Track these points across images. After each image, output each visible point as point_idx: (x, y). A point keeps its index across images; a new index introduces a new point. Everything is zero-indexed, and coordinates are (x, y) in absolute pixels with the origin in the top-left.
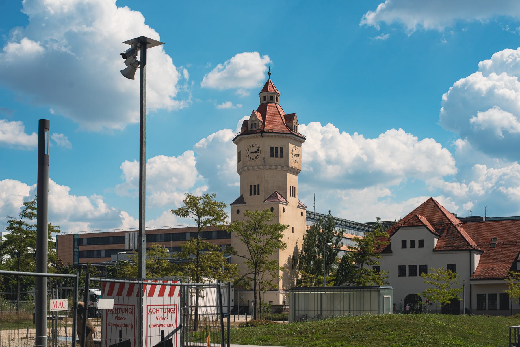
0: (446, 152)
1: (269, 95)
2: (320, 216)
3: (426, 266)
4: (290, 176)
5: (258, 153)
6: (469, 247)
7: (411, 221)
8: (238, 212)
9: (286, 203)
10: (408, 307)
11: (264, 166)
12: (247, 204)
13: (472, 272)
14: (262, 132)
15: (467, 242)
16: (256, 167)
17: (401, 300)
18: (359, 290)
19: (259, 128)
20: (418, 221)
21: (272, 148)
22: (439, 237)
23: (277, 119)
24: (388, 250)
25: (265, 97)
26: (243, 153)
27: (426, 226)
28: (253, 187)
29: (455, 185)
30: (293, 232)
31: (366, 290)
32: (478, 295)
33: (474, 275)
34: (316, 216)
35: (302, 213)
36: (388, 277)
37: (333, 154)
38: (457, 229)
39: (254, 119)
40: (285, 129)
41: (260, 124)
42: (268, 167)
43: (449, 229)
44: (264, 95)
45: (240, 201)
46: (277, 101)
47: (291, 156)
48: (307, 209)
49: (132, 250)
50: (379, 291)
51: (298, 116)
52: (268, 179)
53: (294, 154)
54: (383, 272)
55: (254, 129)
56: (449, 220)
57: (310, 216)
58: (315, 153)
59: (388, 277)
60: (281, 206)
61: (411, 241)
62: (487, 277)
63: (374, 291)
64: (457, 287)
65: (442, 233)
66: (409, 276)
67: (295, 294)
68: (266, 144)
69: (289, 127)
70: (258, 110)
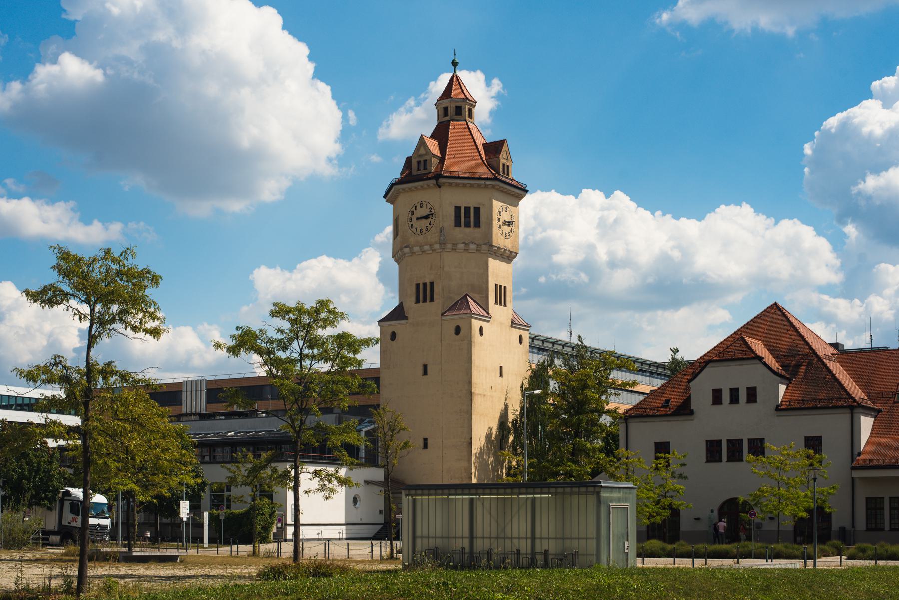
0: (823, 244)
1: (454, 105)
2: (573, 348)
3: (762, 440)
4: (494, 264)
5: (430, 219)
6: (850, 402)
7: (733, 351)
8: (393, 336)
9: (488, 317)
10: (722, 525)
11: (442, 244)
12: (410, 321)
13: (856, 453)
14: (438, 176)
15: (846, 391)
16: (426, 247)
17: (712, 511)
18: (553, 490)
19: (433, 169)
20: (745, 349)
21: (458, 208)
22: (788, 381)
23: (469, 150)
24: (684, 410)
25: (446, 109)
26: (403, 219)
27: (760, 359)
28: (421, 286)
29: (842, 303)
30: (501, 375)
31: (583, 489)
32: (868, 500)
33: (860, 458)
34: (566, 349)
35: (521, 339)
36: (683, 465)
37: (620, 251)
38: (825, 365)
39: (422, 151)
40: (484, 171)
41: (434, 162)
42: (449, 246)
43: (809, 365)
44: (445, 106)
45: (398, 314)
46: (471, 116)
47: (495, 223)
48: (535, 331)
49: (191, 415)
50: (598, 493)
51: (512, 146)
52: (452, 268)
53: (502, 220)
54: (675, 455)
55: (423, 172)
56: (810, 347)
57: (538, 345)
58: (592, 247)
59: (683, 465)
60: (476, 324)
61: (731, 390)
62: (886, 463)
63: (587, 493)
64: (830, 485)
65: (794, 374)
66: (729, 460)
67: (414, 500)
68: (446, 201)
69: (493, 165)
70: (433, 136)
